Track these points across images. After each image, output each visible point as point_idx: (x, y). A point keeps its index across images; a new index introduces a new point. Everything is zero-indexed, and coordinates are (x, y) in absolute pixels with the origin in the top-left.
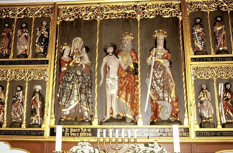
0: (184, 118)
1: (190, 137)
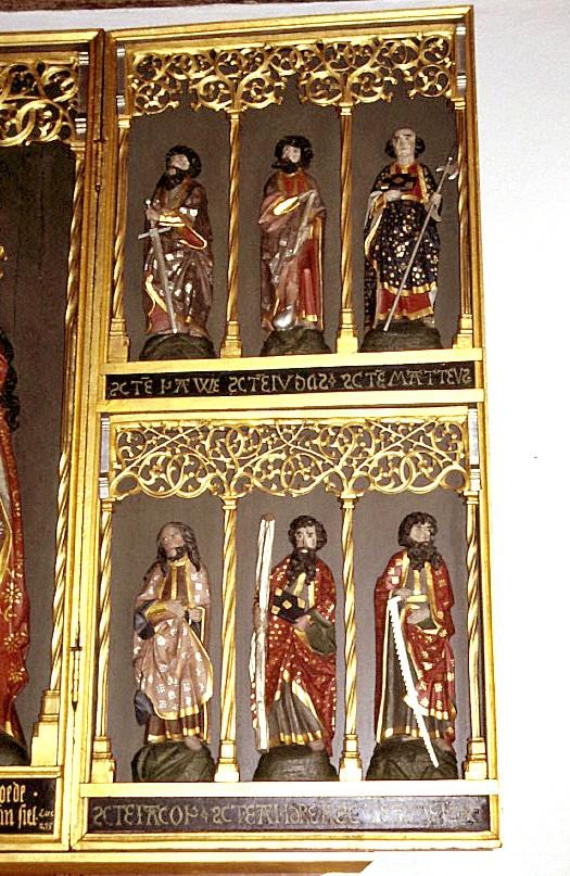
0: (41, 720)
1: (56, 835)
